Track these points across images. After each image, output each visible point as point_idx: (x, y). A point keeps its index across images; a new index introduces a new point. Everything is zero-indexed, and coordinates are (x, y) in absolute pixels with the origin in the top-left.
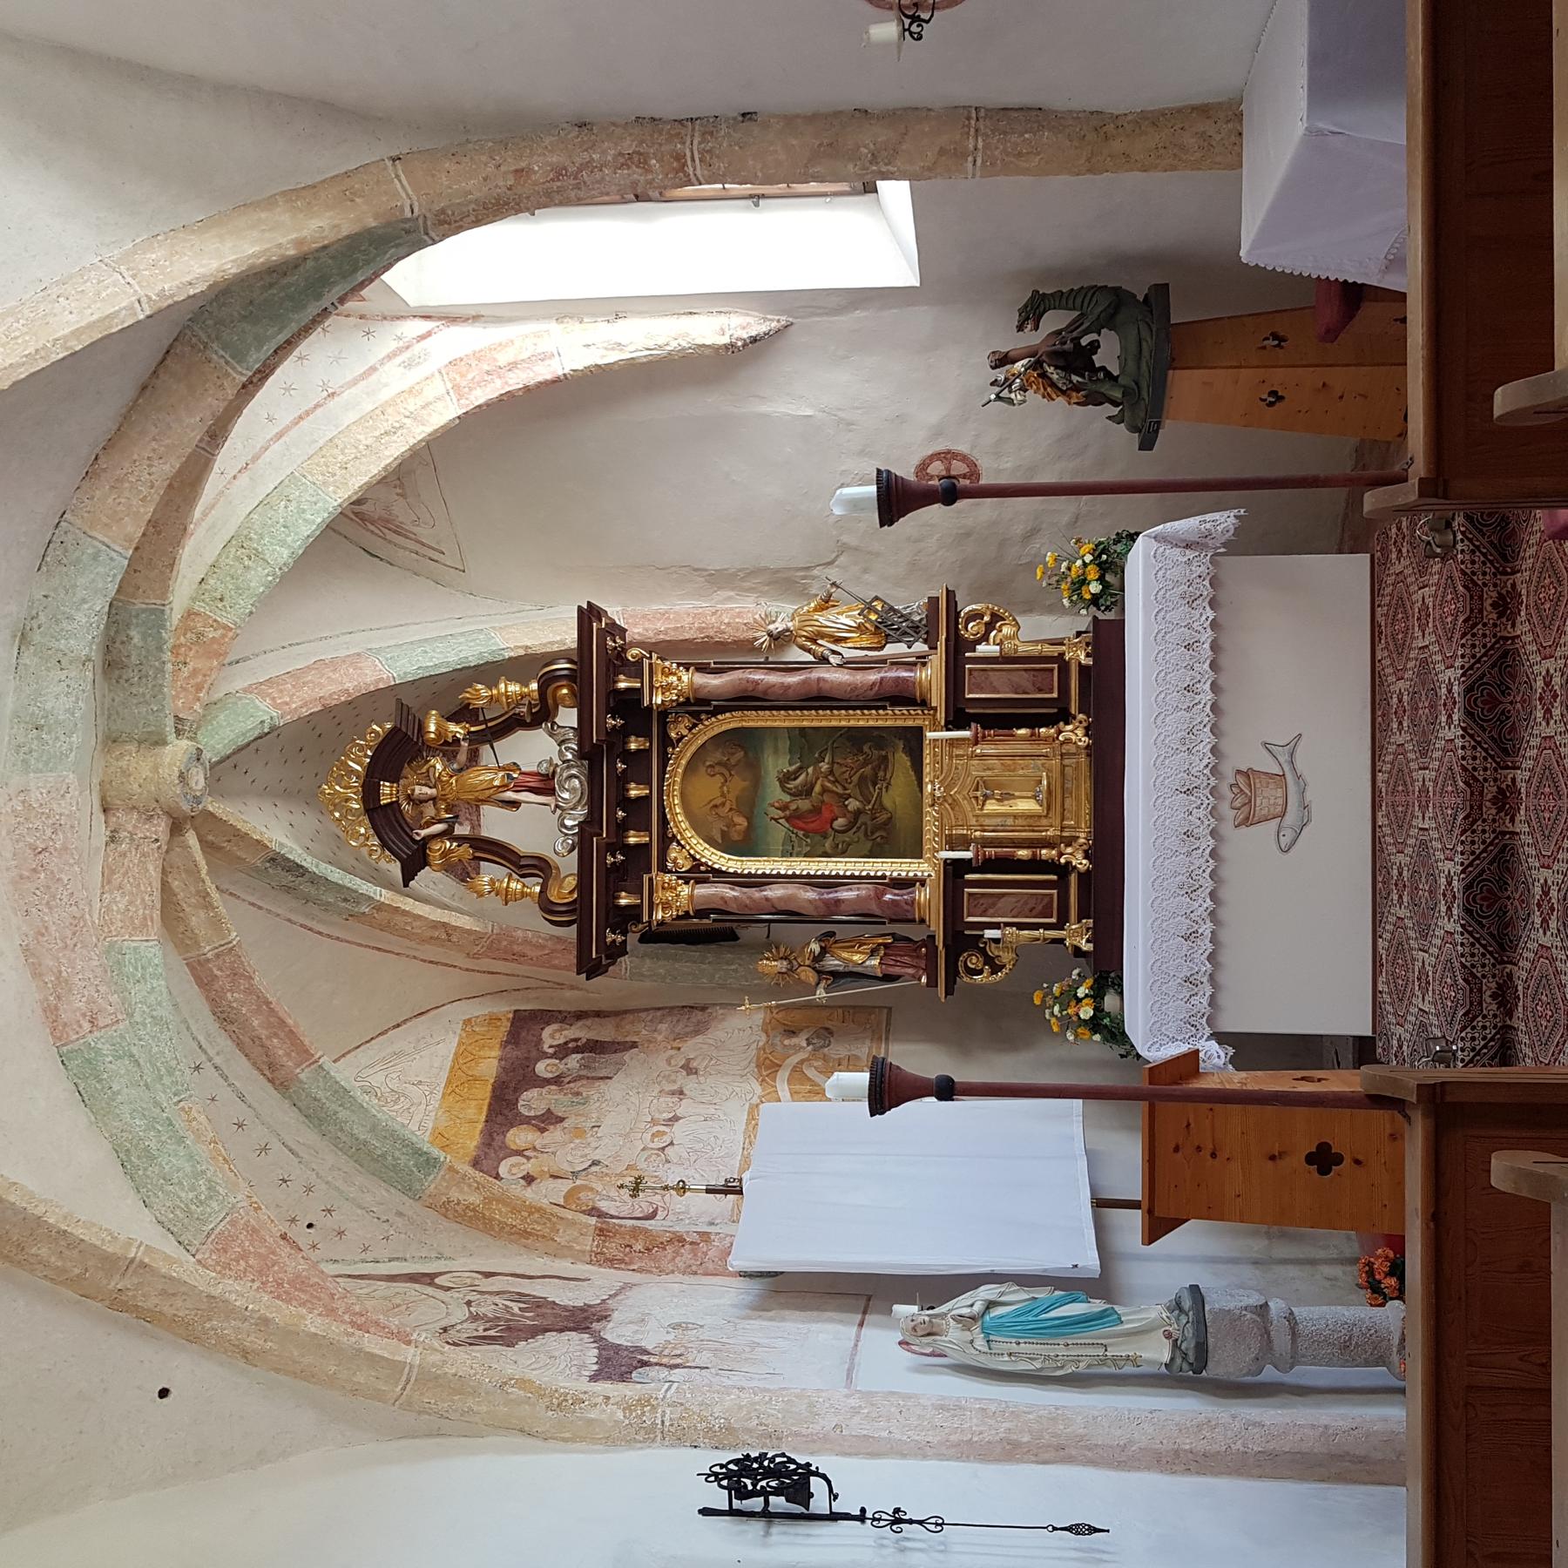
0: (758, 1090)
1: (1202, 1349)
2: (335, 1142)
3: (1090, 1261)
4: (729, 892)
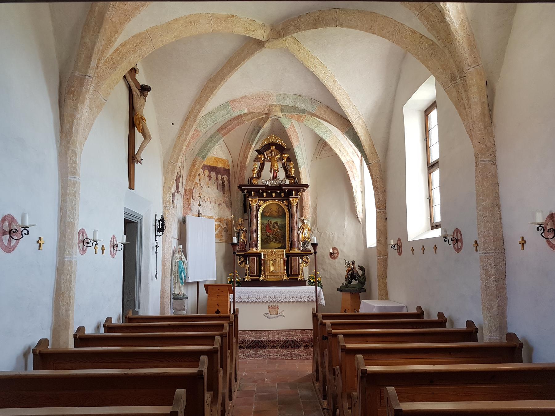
0: (216, 218)
1: (178, 299)
2: (207, 140)
3: (190, 280)
4: (254, 213)
